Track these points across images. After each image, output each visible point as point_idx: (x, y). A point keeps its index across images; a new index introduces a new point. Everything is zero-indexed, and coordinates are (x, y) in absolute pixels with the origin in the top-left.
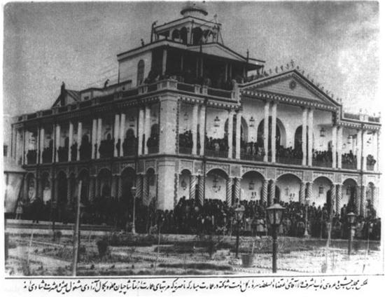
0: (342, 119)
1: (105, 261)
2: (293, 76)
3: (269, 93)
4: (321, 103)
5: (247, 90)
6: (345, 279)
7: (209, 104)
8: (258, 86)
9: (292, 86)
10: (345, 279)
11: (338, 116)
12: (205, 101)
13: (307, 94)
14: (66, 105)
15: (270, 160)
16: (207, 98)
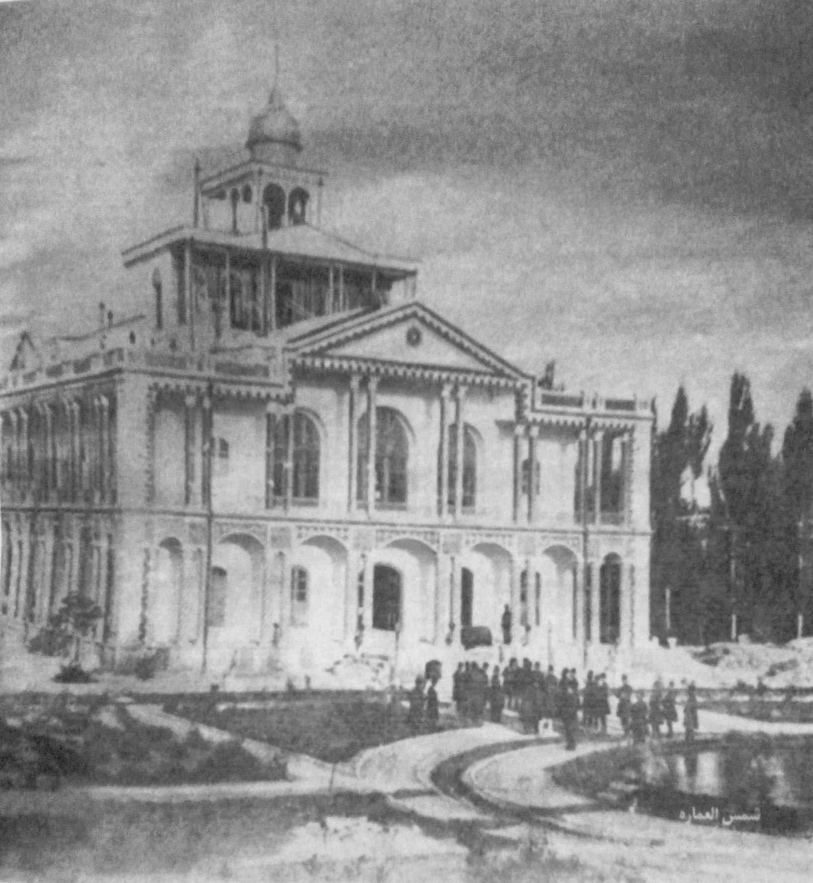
0: (533, 410)
1: (93, 497)
2: (415, 315)
3: (349, 358)
4: (485, 374)
5: (304, 355)
6: (331, 671)
7: (219, 391)
8: (330, 346)
9: (414, 339)
10: (331, 671)
11: (528, 402)
12: (210, 388)
13: (450, 357)
14: (94, 718)
15: (459, 439)
16: (211, 382)
